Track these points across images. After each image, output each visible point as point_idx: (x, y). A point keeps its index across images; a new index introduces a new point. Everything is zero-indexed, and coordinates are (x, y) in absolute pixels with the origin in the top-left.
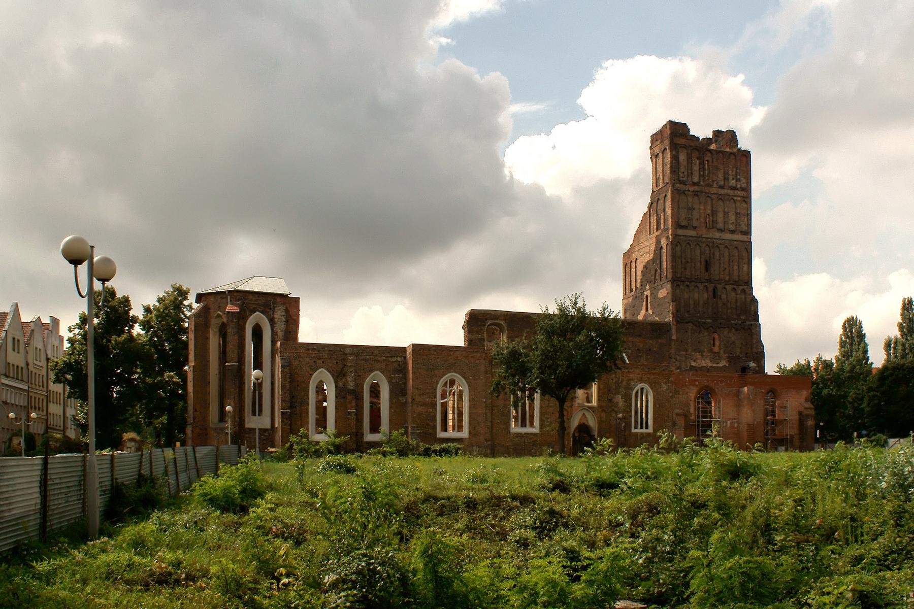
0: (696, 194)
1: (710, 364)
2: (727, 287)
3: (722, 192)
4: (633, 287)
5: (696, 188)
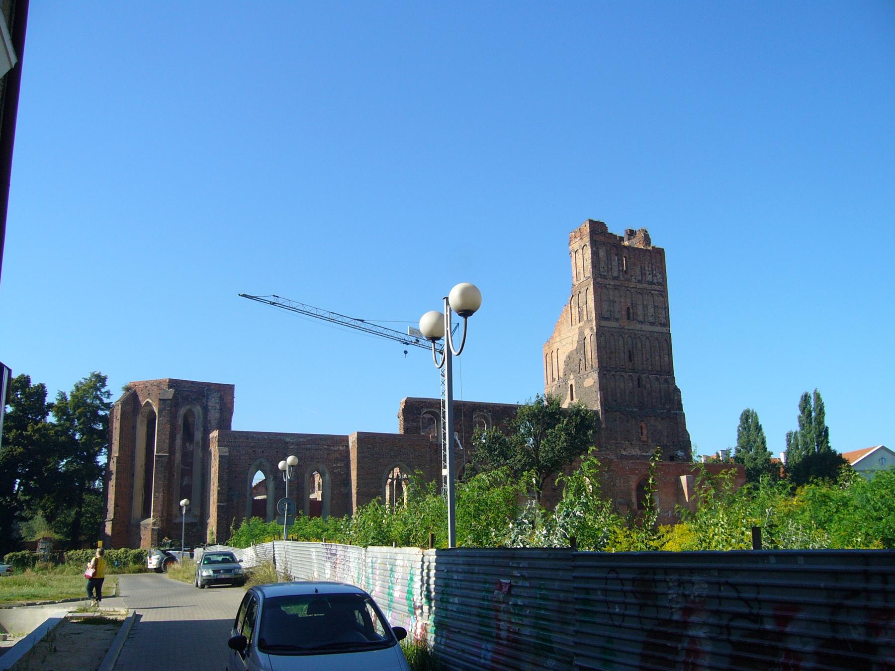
0: (616, 288)
1: (639, 453)
2: (651, 377)
3: (639, 286)
4: (555, 376)
5: (616, 282)
